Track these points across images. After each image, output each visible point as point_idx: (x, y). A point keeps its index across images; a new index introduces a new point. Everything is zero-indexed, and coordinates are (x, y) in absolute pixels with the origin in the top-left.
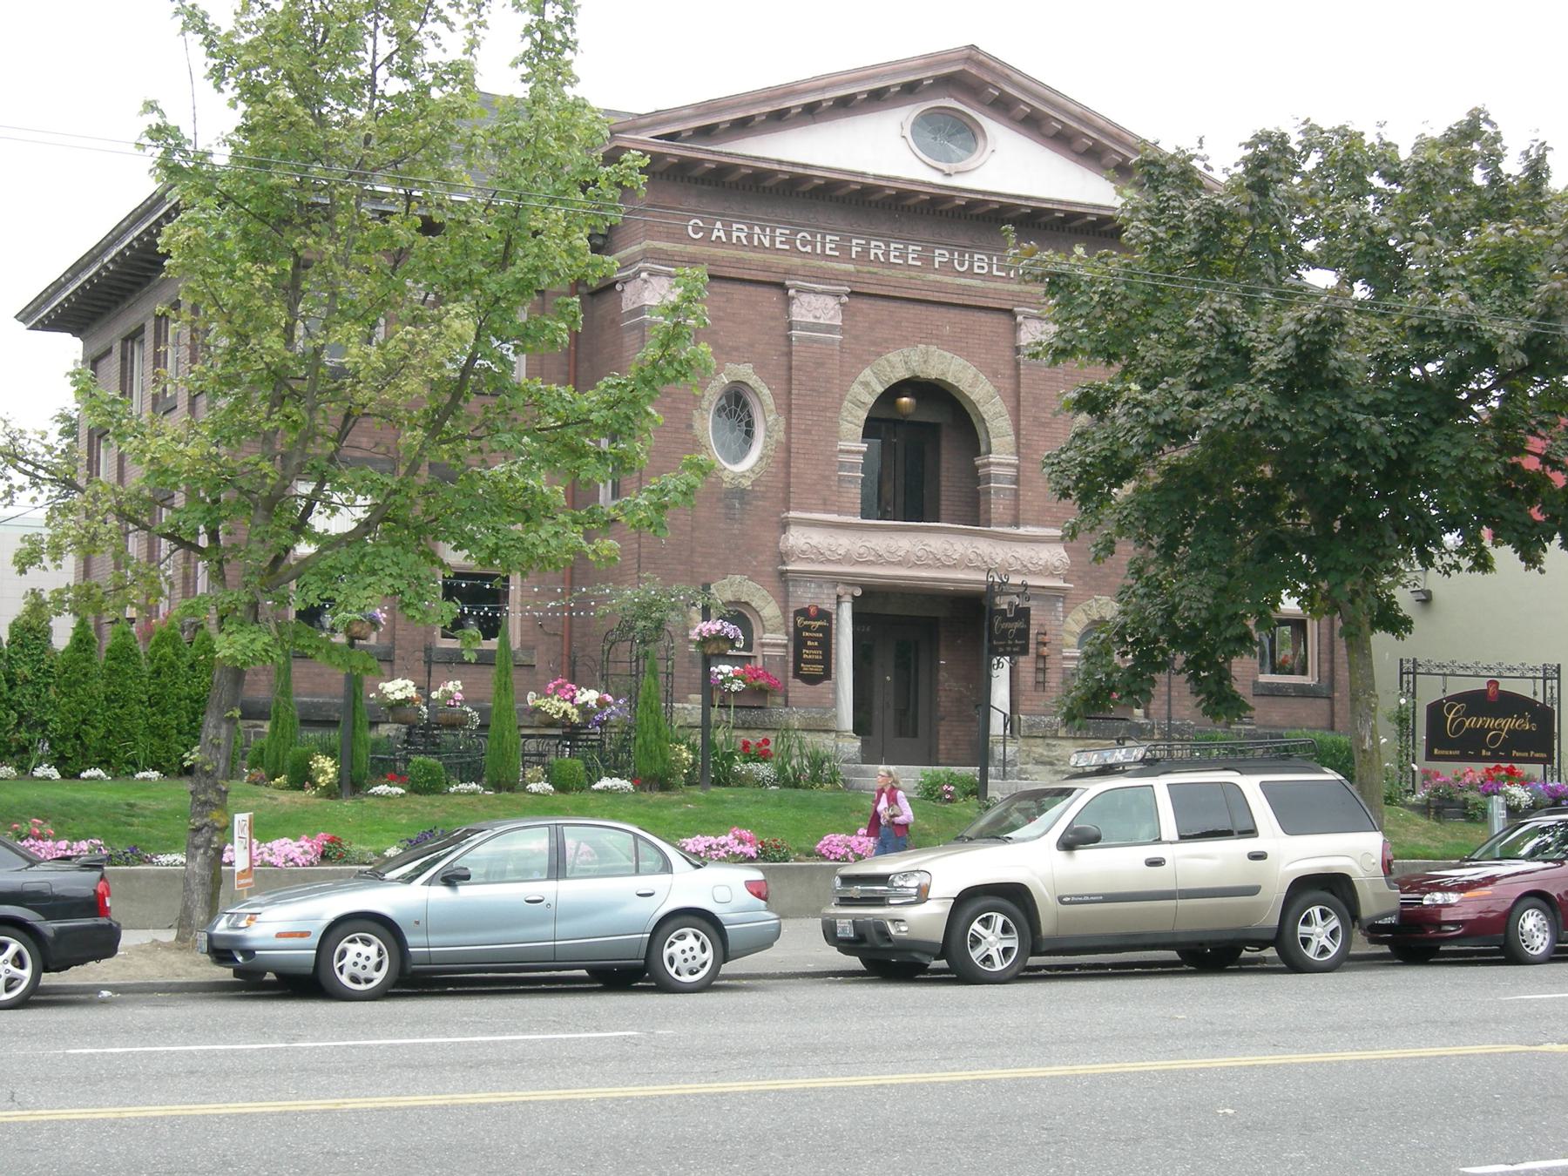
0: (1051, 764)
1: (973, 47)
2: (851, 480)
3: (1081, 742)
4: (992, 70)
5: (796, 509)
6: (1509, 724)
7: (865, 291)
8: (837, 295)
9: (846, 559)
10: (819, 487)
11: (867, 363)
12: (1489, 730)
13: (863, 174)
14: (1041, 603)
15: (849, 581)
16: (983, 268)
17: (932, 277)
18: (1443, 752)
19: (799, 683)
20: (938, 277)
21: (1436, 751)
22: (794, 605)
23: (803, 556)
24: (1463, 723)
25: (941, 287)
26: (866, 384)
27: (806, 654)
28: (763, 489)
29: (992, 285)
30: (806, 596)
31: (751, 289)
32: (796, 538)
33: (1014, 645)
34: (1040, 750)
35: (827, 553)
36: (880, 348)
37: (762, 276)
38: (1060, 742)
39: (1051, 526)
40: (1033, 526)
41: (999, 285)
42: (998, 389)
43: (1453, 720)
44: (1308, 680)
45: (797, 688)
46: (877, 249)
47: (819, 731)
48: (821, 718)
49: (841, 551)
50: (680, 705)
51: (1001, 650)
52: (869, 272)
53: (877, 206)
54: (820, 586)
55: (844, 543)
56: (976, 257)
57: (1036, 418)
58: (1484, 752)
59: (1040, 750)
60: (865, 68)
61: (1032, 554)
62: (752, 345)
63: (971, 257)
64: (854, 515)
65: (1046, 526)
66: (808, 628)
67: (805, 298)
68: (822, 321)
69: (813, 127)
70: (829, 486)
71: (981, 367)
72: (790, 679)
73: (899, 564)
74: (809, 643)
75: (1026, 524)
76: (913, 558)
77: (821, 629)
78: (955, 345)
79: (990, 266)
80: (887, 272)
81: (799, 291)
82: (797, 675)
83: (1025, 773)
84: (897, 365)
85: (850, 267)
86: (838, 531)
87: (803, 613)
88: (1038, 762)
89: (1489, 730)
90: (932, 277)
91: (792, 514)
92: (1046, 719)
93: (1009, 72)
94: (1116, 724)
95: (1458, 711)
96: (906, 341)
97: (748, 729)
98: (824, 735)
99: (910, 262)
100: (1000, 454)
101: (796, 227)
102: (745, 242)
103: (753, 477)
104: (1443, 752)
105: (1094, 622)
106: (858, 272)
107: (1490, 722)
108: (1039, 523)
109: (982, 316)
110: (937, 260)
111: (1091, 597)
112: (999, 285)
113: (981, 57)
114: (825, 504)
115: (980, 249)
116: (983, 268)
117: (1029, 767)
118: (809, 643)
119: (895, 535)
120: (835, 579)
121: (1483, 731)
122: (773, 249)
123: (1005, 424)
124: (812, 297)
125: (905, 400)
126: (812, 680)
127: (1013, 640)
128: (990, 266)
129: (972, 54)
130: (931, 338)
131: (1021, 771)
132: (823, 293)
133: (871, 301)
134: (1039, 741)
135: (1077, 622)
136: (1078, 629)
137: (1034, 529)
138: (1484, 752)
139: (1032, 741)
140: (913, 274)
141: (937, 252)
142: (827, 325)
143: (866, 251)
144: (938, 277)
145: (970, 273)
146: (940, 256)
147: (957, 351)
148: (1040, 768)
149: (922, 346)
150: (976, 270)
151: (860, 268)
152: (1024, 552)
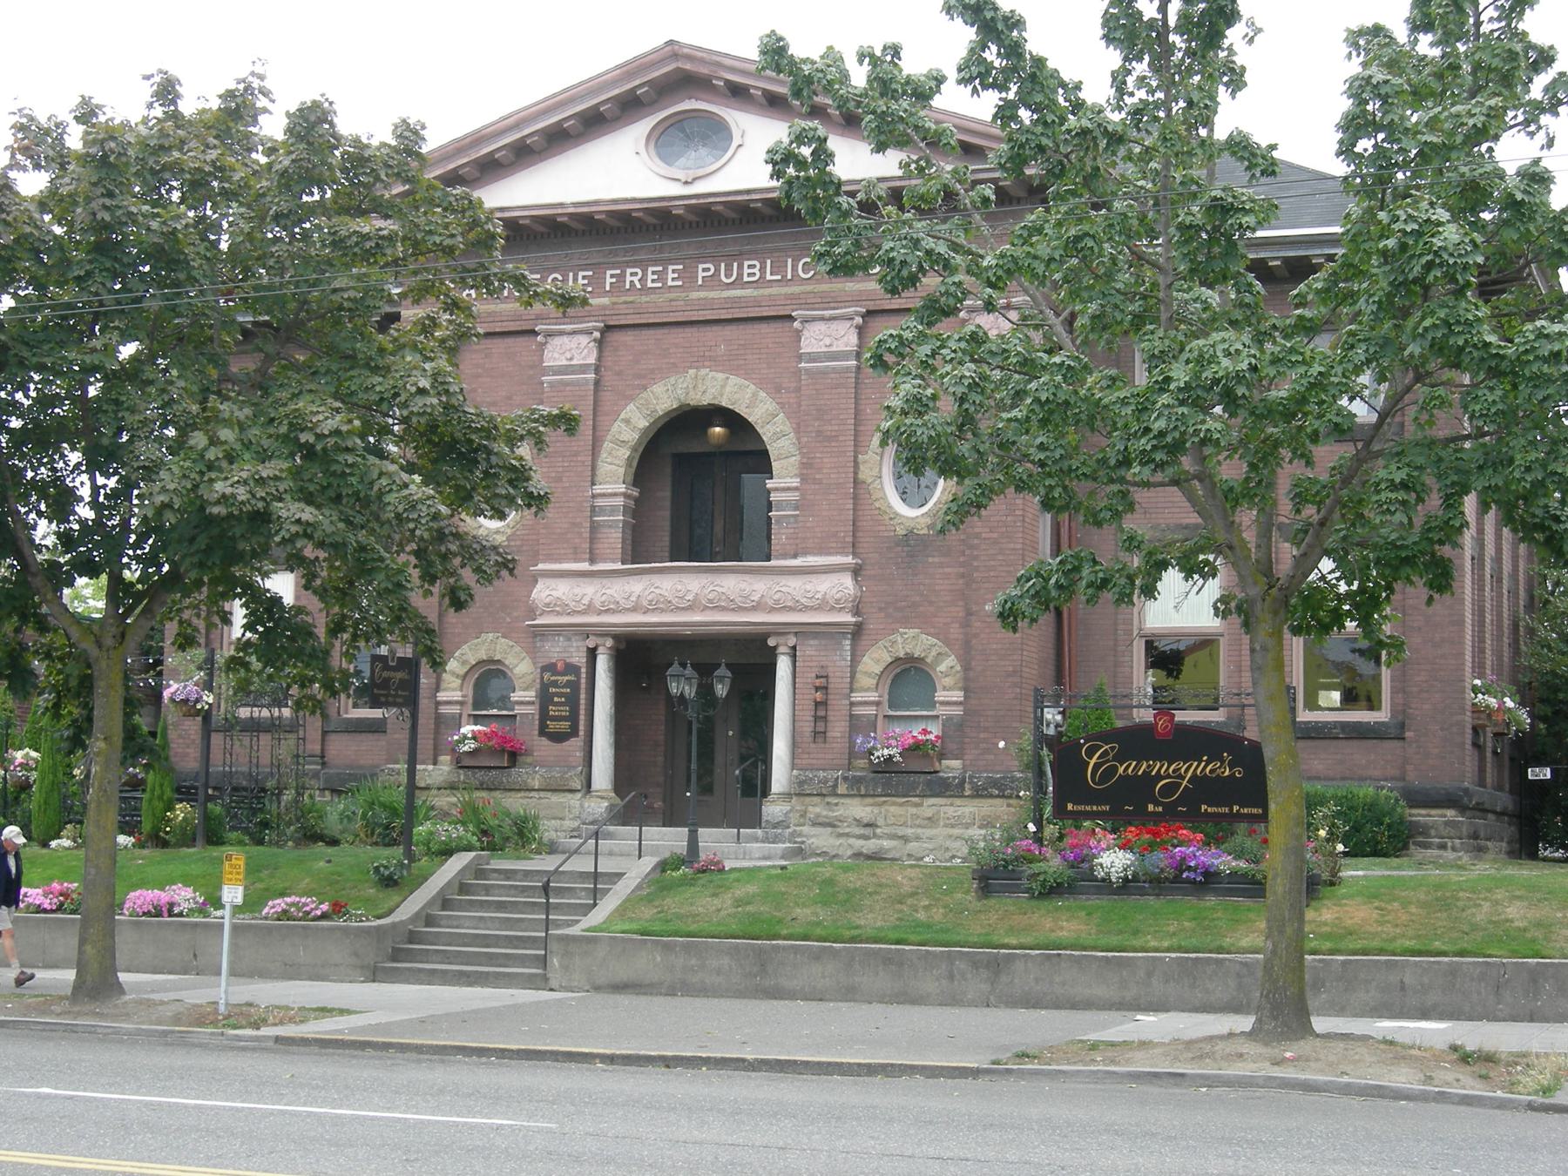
0: (834, 826)
1: (671, 42)
2: (611, 525)
3: (870, 800)
4: (702, 61)
5: (544, 561)
6: (1190, 770)
7: (622, 322)
8: (589, 332)
9: (590, 609)
10: (569, 536)
11: (631, 399)
12: (1159, 777)
13: (561, 205)
14: (823, 642)
15: (601, 632)
16: (754, 274)
17: (695, 295)
18: (1081, 808)
19: (545, 741)
20: (702, 294)
21: (1070, 807)
22: (543, 661)
23: (551, 608)
24: (1114, 769)
25: (706, 304)
26: (627, 421)
27: (553, 711)
28: (518, 543)
29: (767, 291)
30: (556, 650)
31: (510, 341)
32: (542, 592)
33: (396, 696)
34: (818, 810)
35: (803, 600)
36: (644, 380)
37: (513, 327)
38: (842, 801)
39: (837, 553)
40: (815, 554)
41: (774, 290)
42: (782, 405)
43: (1097, 766)
44: (1381, 716)
45: (543, 747)
46: (633, 277)
47: (564, 791)
48: (562, 777)
49: (690, 597)
50: (423, 767)
51: (383, 699)
52: (626, 303)
53: (691, 226)
54: (569, 640)
55: (589, 591)
56: (746, 263)
57: (819, 433)
58: (1151, 807)
59: (818, 810)
60: (554, 96)
61: (743, 585)
62: (510, 398)
63: (740, 267)
64: (613, 561)
65: (829, 554)
66: (555, 684)
67: (557, 341)
68: (574, 362)
69: (541, 165)
70: (580, 534)
71: (761, 384)
72: (536, 738)
73: (634, 609)
74: (556, 699)
75: (605, 560)
76: (770, 603)
77: (569, 682)
78: (731, 365)
79: (762, 270)
80: (644, 299)
81: (806, 321)
82: (543, 732)
83: (800, 835)
84: (664, 397)
85: (605, 301)
86: (586, 580)
87: (550, 668)
88: (814, 824)
89: (1159, 777)
90: (695, 295)
91: (541, 566)
92: (821, 774)
93: (718, 59)
94: (912, 778)
95: (1105, 753)
96: (675, 368)
97: (490, 790)
98: (570, 796)
99: (670, 283)
100: (784, 479)
101: (691, 262)
102: (639, 286)
103: (509, 531)
104: (1081, 808)
105: (898, 659)
106: (614, 304)
107: (1158, 767)
108: (822, 551)
109: (764, 328)
110: (701, 274)
111: (894, 631)
112: (774, 290)
113: (686, 51)
114: (576, 553)
115: (752, 254)
116: (749, 267)
117: (805, 829)
118: (556, 699)
119: (632, 579)
120: (584, 631)
121: (1149, 780)
122: (645, 290)
123: (788, 442)
124: (565, 339)
125: (718, 429)
126: (558, 738)
127: (395, 690)
128: (762, 270)
129: (673, 50)
130: (700, 361)
131: (793, 834)
132: (574, 333)
133: (637, 332)
134: (816, 800)
135: (877, 661)
136: (878, 669)
137: (816, 559)
138: (1151, 807)
139: (808, 799)
140: (672, 296)
141: (701, 266)
142: (581, 365)
143: (621, 277)
144: (702, 294)
145: (739, 283)
146: (703, 270)
147: (735, 371)
148: (820, 830)
149: (692, 372)
150: (746, 279)
151: (614, 300)
152: (795, 587)
